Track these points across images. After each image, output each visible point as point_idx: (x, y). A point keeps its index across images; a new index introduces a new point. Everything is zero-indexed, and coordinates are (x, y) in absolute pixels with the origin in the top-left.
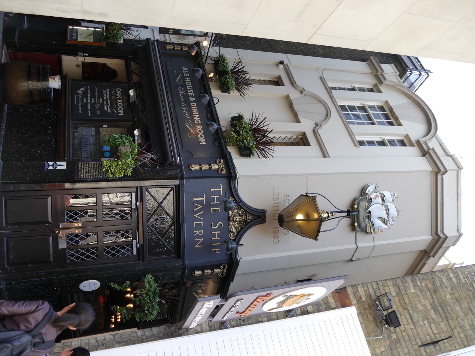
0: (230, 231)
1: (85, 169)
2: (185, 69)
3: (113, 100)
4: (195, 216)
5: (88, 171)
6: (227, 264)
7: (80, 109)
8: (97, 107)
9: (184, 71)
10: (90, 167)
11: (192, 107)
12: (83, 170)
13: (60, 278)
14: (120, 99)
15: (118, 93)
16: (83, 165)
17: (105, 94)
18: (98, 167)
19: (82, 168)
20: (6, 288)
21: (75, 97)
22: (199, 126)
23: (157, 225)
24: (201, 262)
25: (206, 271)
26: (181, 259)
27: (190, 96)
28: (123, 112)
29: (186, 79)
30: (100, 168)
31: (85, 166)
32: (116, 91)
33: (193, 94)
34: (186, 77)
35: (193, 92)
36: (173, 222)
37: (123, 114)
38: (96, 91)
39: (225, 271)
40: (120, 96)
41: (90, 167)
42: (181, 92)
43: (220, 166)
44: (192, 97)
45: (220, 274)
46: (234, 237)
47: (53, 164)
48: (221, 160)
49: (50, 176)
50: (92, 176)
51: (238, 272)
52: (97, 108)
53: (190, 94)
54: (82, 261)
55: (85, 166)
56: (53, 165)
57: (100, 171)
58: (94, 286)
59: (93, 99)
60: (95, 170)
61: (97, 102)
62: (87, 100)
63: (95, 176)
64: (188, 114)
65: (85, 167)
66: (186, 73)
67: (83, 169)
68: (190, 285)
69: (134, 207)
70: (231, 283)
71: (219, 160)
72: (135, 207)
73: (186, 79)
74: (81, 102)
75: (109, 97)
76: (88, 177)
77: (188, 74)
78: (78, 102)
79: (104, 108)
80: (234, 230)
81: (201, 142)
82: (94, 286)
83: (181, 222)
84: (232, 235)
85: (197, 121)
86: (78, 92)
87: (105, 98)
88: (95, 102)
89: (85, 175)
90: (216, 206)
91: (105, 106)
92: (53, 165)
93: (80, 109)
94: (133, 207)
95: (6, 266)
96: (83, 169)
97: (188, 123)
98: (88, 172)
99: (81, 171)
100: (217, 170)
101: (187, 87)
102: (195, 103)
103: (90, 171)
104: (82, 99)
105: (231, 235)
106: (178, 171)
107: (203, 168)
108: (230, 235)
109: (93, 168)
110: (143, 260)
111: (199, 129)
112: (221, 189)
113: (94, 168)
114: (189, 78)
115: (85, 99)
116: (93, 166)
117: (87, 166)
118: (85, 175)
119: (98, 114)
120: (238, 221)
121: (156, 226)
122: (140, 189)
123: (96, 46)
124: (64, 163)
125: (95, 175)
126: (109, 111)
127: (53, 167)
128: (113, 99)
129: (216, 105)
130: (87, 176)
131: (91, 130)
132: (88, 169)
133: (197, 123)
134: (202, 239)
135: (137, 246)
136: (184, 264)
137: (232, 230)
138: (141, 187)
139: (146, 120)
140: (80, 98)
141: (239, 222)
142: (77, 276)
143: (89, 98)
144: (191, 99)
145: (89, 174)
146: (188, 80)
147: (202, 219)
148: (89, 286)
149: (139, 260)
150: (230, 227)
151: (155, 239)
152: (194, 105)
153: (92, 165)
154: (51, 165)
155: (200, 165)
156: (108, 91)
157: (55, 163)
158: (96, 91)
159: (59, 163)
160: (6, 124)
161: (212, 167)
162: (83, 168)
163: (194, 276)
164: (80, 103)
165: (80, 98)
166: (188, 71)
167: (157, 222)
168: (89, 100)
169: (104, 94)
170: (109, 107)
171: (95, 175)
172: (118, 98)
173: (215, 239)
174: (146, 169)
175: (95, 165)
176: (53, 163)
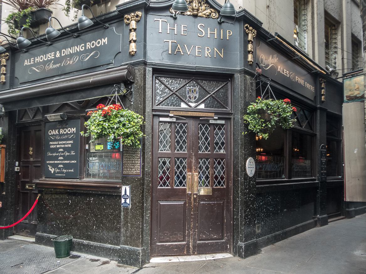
0: (208, 16)
1: (130, 167)
2: (26, 63)
3: (60, 138)
4: (189, 53)
5: (132, 165)
6: (244, 25)
7: (70, 171)
8: (67, 154)
9: (29, 64)
10: (128, 162)
11: (67, 54)
12: (131, 169)
13: (240, 195)
14: (59, 132)
15: (53, 133)
16: (126, 169)
17: (55, 146)
18: (128, 154)
19: (130, 170)
20: (244, 242)
21: (58, 175)
22: (87, 46)
23: (195, 97)
24: (239, 52)
25: (249, 49)
26: (234, 74)
27: (55, 56)
28: (72, 128)
29: (37, 61)
30: (129, 152)
31: (127, 167)
32: (51, 135)
33: (52, 53)
34: (34, 62)
35: (50, 54)
36: (194, 80)
37: (75, 128)
38: (51, 155)
39: (251, 28)
40: (57, 132)
41: (128, 162)
42: (51, 67)
43: (133, 19)
44: (55, 54)
45: (253, 34)
46: (216, 12)
47: (124, 198)
48: (126, 18)
49: (136, 202)
50: (138, 160)
51: (254, 14)
52: (69, 154)
53: (53, 56)
54: (226, 173)
55: (127, 167)
56: (125, 199)
57: (133, 152)
58: (251, 163)
59: (60, 158)
60: (132, 157)
61: (62, 154)
62: (61, 164)
63: (138, 157)
64: (74, 59)
65: (128, 167)
66: (30, 62)
67: (130, 170)
68: (261, 70)
69: (174, 120)
70: (263, 26)
71: (126, 21)
72: (175, 119)
73: (37, 61)
74: (63, 169)
75: (58, 142)
76: (139, 165)
77: (32, 59)
78: (63, 173)
79: (69, 147)
80: (208, 11)
81: (104, 43)
82: (251, 163)
83: (195, 70)
84: (214, 15)
85: (82, 48)
86: (52, 172)
87: (58, 146)
88: (63, 156)
89: (136, 167)
90: (179, 29)
91: (67, 146)
92: (125, 199)
93: (70, 171)
94: (175, 121)
95: (224, 241)
96: (130, 170)
97: (83, 58)
98: (134, 164)
99: (133, 171)
100: (138, 22)
101: (45, 60)
102: (63, 50)
103: (132, 162)
104: (59, 168)
105: (213, 15)
106: (136, 68)
107: (134, 39)
108: (213, 17)
109: (129, 159)
110: (231, 114)
111: (90, 46)
112: (161, 20)
113: (130, 159)
114: (36, 58)
115: (60, 166)
116: (128, 159)
117: (128, 165)
118: (136, 167)
119: (74, 154)
120: (198, 5)
121: (197, 98)
122: (155, 112)
123: (6, 154)
124: (123, 188)
125: (137, 158)
126: (71, 142)
127: (127, 199)
128: (59, 138)
129: (63, 27)
130: (138, 165)
131: (91, 161)
132: (131, 164)
133: (83, 48)
134: (215, 49)
135: (216, 120)
136: (240, 72)
137: (208, 14)
138: (153, 110)
139: (81, 104)
140: (59, 171)
141: (200, 4)
142: (241, 179)
143: (58, 162)
144: (58, 55)
145: (136, 164)
146: (38, 59)
147: (193, 46)
148: (251, 168)
149: (230, 119)
150: (205, 15)
151: (209, 101)
152: (64, 52)
153: (126, 160)
154: (125, 201)
155: (130, 42)
156: (51, 143)
157: (123, 197)
158: (51, 155)
159: (123, 193)
160: (84, 240)
161: (133, 29)
162: (129, 169)
163: (253, 62)
164: (63, 171)
165: (59, 171)
166: (29, 60)
167: (192, 98)
168: (60, 161)
169: (55, 147)
170: (67, 142)
171: (137, 158)
172: (58, 134)
173: (216, 34)
174: (134, 103)
175: (126, 157)
176: (123, 198)
